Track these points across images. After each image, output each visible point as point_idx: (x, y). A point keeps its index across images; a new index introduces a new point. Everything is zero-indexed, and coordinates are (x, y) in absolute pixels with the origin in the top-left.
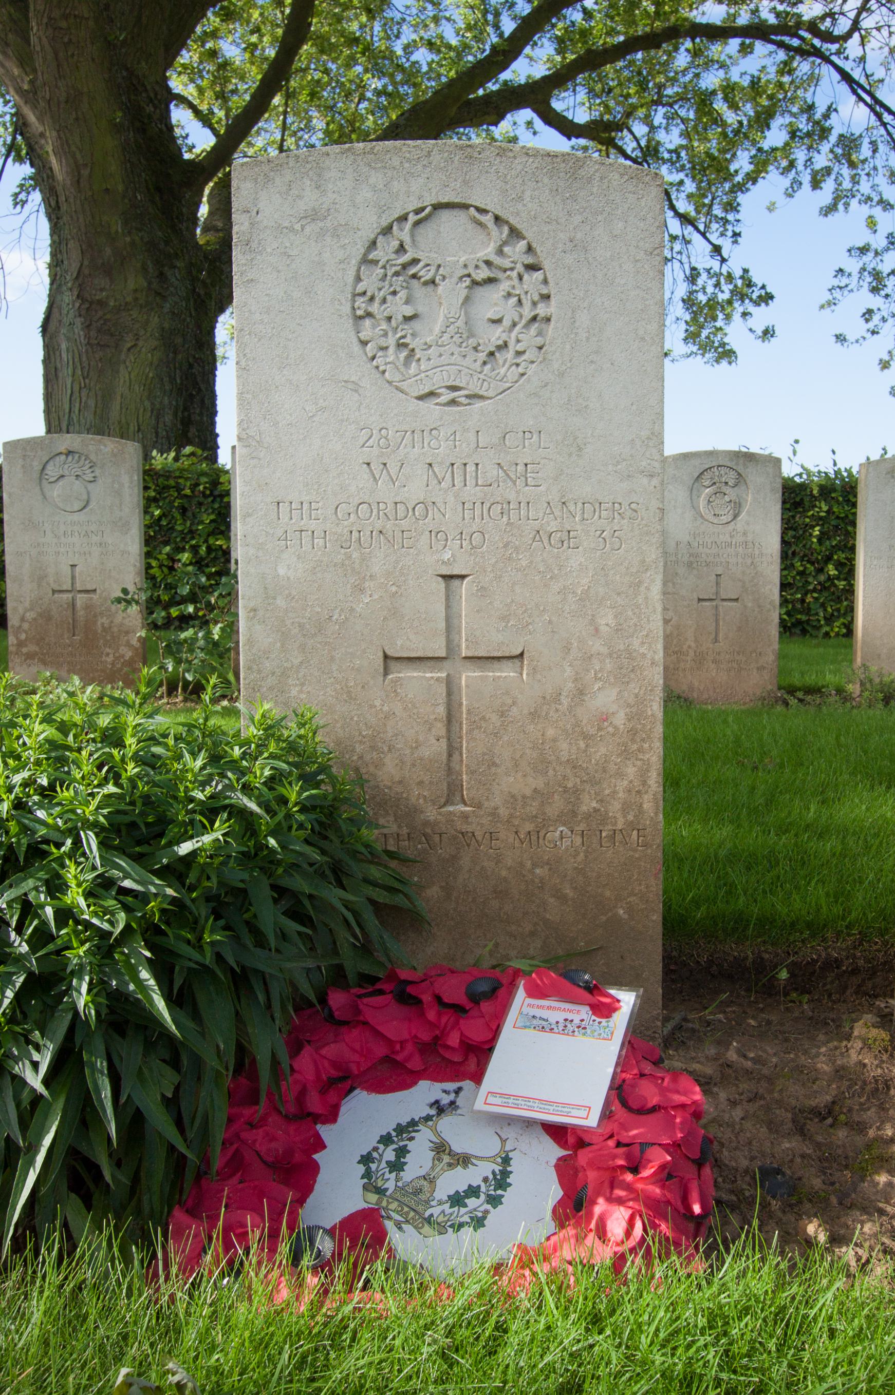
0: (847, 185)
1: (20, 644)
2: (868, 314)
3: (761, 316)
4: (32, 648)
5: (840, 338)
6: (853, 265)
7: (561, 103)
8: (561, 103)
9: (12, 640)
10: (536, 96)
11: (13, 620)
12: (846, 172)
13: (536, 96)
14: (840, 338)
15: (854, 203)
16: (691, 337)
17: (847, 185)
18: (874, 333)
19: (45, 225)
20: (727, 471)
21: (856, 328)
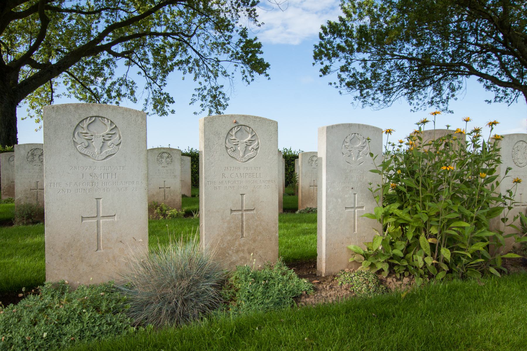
0: (197, 72)
1: (4, 192)
2: (202, 105)
3: (172, 106)
4: (7, 193)
5: (195, 113)
6: (197, 93)
7: (113, 48)
8: (113, 48)
9: (2, 191)
10: (107, 48)
11: (2, 188)
12: (197, 68)
13: (107, 48)
14: (195, 113)
15: (200, 76)
16: (155, 107)
17: (197, 72)
18: (203, 110)
19: (524, 97)
20: (165, 154)
21: (199, 109)
